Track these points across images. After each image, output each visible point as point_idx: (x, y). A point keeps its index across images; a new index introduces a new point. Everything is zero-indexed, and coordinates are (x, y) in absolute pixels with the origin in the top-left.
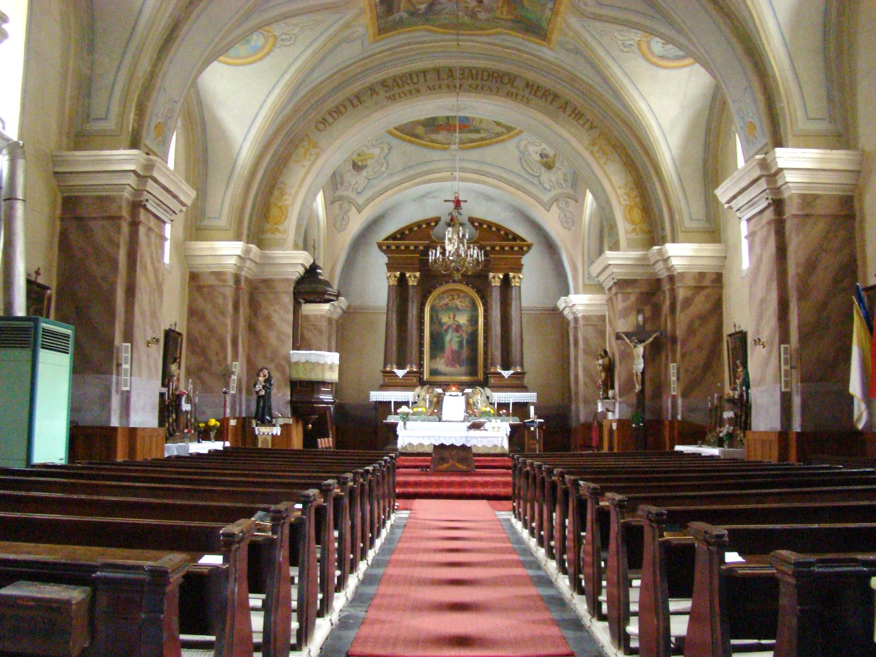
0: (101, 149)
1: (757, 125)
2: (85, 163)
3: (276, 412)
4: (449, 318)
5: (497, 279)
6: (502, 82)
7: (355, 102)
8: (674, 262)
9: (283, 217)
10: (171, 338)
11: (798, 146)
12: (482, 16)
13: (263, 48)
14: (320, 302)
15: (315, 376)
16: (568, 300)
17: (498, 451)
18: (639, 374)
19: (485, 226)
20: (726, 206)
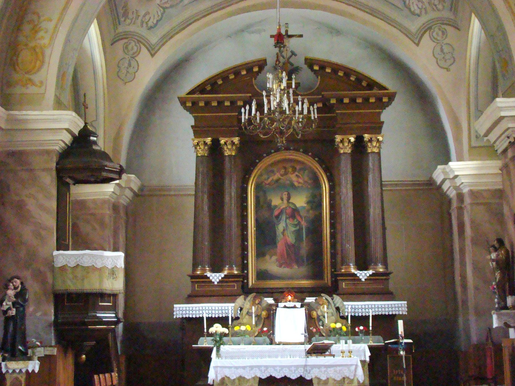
3: (32, 340)
4: (282, 199)
5: (346, 144)
9: (38, 62)
16: (448, 170)
19: (328, 70)
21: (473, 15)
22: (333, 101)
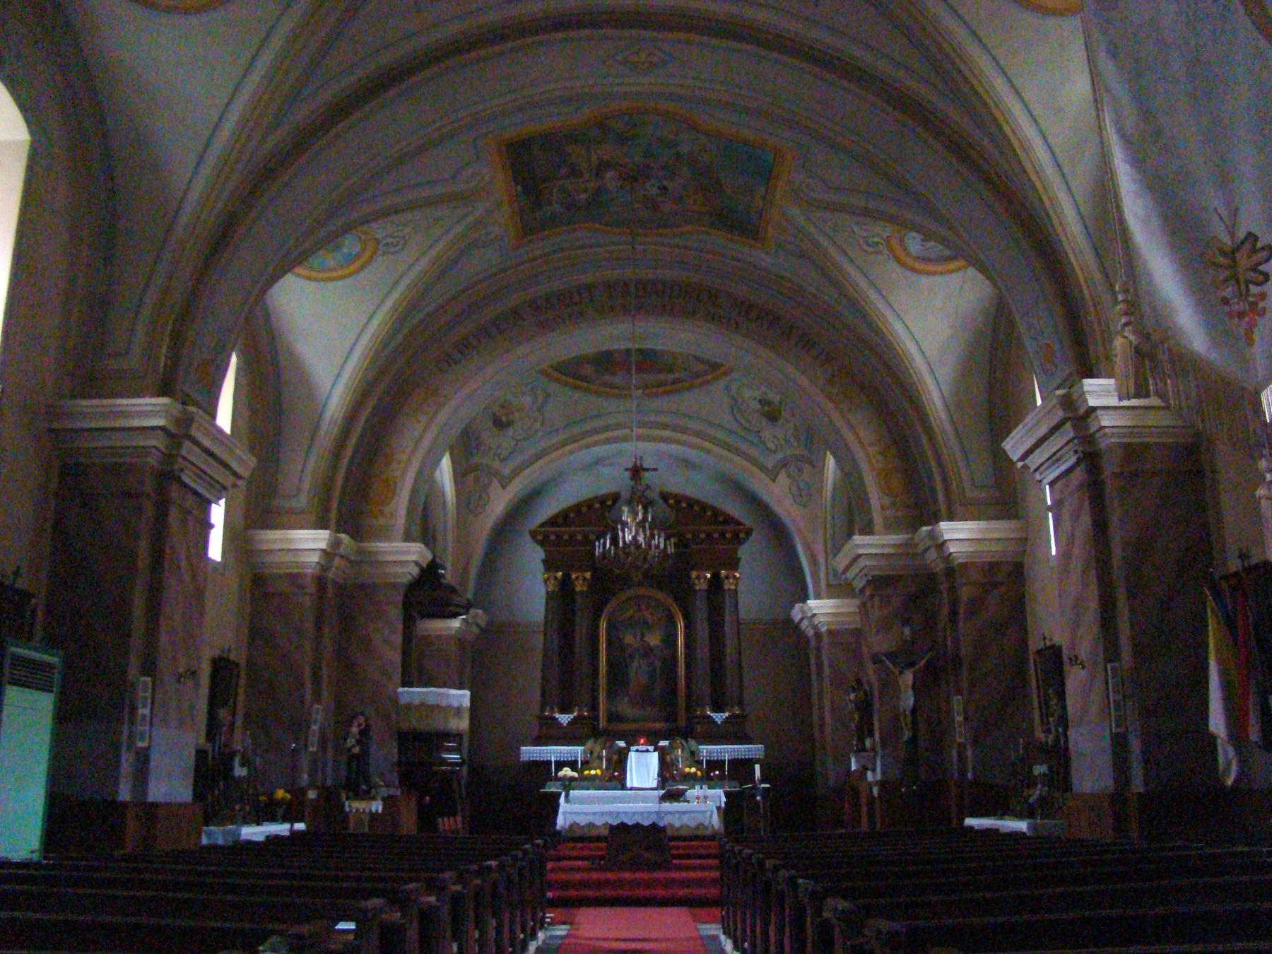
0: (114, 395)
3: (376, 779)
4: (635, 637)
10: (222, 667)
12: (667, 208)
13: (358, 256)
15: (436, 724)
16: (806, 609)
17: (709, 832)
18: (908, 712)
19: (684, 505)
20: (1020, 465)
22: (689, 536)
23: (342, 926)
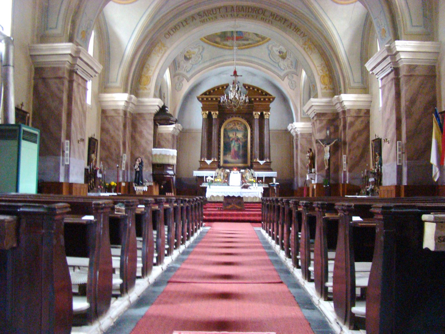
0: (53, 42)
1: (387, 30)
2: (46, 50)
3: (145, 180)
5: (257, 115)
6: (258, 13)
7: (184, 24)
8: (345, 104)
10: (92, 142)
11: (407, 40)
14: (167, 125)
15: (165, 161)
18: (327, 161)
20: (371, 72)
21: (303, 70)
22: (253, 99)
23: (139, 206)
